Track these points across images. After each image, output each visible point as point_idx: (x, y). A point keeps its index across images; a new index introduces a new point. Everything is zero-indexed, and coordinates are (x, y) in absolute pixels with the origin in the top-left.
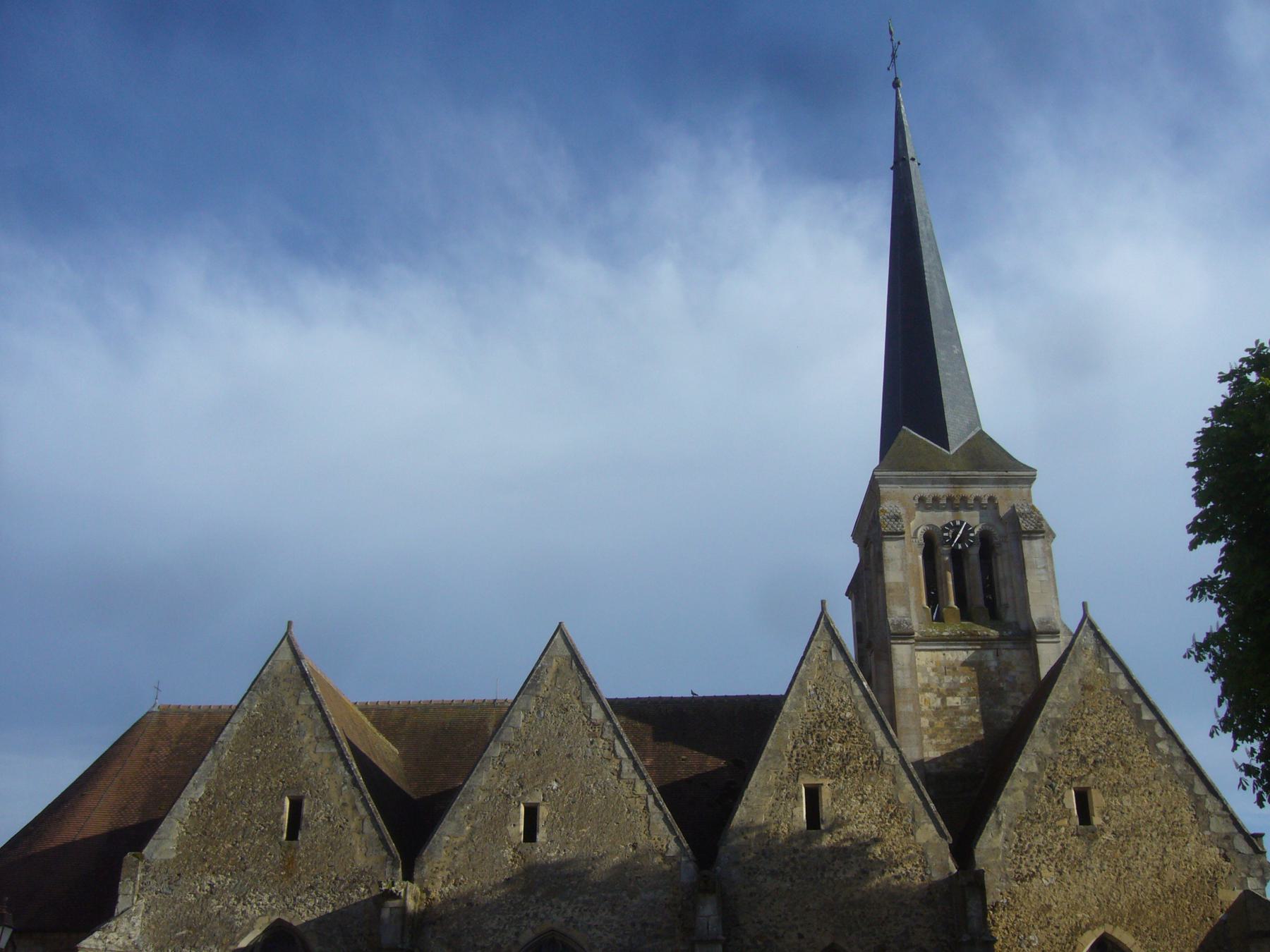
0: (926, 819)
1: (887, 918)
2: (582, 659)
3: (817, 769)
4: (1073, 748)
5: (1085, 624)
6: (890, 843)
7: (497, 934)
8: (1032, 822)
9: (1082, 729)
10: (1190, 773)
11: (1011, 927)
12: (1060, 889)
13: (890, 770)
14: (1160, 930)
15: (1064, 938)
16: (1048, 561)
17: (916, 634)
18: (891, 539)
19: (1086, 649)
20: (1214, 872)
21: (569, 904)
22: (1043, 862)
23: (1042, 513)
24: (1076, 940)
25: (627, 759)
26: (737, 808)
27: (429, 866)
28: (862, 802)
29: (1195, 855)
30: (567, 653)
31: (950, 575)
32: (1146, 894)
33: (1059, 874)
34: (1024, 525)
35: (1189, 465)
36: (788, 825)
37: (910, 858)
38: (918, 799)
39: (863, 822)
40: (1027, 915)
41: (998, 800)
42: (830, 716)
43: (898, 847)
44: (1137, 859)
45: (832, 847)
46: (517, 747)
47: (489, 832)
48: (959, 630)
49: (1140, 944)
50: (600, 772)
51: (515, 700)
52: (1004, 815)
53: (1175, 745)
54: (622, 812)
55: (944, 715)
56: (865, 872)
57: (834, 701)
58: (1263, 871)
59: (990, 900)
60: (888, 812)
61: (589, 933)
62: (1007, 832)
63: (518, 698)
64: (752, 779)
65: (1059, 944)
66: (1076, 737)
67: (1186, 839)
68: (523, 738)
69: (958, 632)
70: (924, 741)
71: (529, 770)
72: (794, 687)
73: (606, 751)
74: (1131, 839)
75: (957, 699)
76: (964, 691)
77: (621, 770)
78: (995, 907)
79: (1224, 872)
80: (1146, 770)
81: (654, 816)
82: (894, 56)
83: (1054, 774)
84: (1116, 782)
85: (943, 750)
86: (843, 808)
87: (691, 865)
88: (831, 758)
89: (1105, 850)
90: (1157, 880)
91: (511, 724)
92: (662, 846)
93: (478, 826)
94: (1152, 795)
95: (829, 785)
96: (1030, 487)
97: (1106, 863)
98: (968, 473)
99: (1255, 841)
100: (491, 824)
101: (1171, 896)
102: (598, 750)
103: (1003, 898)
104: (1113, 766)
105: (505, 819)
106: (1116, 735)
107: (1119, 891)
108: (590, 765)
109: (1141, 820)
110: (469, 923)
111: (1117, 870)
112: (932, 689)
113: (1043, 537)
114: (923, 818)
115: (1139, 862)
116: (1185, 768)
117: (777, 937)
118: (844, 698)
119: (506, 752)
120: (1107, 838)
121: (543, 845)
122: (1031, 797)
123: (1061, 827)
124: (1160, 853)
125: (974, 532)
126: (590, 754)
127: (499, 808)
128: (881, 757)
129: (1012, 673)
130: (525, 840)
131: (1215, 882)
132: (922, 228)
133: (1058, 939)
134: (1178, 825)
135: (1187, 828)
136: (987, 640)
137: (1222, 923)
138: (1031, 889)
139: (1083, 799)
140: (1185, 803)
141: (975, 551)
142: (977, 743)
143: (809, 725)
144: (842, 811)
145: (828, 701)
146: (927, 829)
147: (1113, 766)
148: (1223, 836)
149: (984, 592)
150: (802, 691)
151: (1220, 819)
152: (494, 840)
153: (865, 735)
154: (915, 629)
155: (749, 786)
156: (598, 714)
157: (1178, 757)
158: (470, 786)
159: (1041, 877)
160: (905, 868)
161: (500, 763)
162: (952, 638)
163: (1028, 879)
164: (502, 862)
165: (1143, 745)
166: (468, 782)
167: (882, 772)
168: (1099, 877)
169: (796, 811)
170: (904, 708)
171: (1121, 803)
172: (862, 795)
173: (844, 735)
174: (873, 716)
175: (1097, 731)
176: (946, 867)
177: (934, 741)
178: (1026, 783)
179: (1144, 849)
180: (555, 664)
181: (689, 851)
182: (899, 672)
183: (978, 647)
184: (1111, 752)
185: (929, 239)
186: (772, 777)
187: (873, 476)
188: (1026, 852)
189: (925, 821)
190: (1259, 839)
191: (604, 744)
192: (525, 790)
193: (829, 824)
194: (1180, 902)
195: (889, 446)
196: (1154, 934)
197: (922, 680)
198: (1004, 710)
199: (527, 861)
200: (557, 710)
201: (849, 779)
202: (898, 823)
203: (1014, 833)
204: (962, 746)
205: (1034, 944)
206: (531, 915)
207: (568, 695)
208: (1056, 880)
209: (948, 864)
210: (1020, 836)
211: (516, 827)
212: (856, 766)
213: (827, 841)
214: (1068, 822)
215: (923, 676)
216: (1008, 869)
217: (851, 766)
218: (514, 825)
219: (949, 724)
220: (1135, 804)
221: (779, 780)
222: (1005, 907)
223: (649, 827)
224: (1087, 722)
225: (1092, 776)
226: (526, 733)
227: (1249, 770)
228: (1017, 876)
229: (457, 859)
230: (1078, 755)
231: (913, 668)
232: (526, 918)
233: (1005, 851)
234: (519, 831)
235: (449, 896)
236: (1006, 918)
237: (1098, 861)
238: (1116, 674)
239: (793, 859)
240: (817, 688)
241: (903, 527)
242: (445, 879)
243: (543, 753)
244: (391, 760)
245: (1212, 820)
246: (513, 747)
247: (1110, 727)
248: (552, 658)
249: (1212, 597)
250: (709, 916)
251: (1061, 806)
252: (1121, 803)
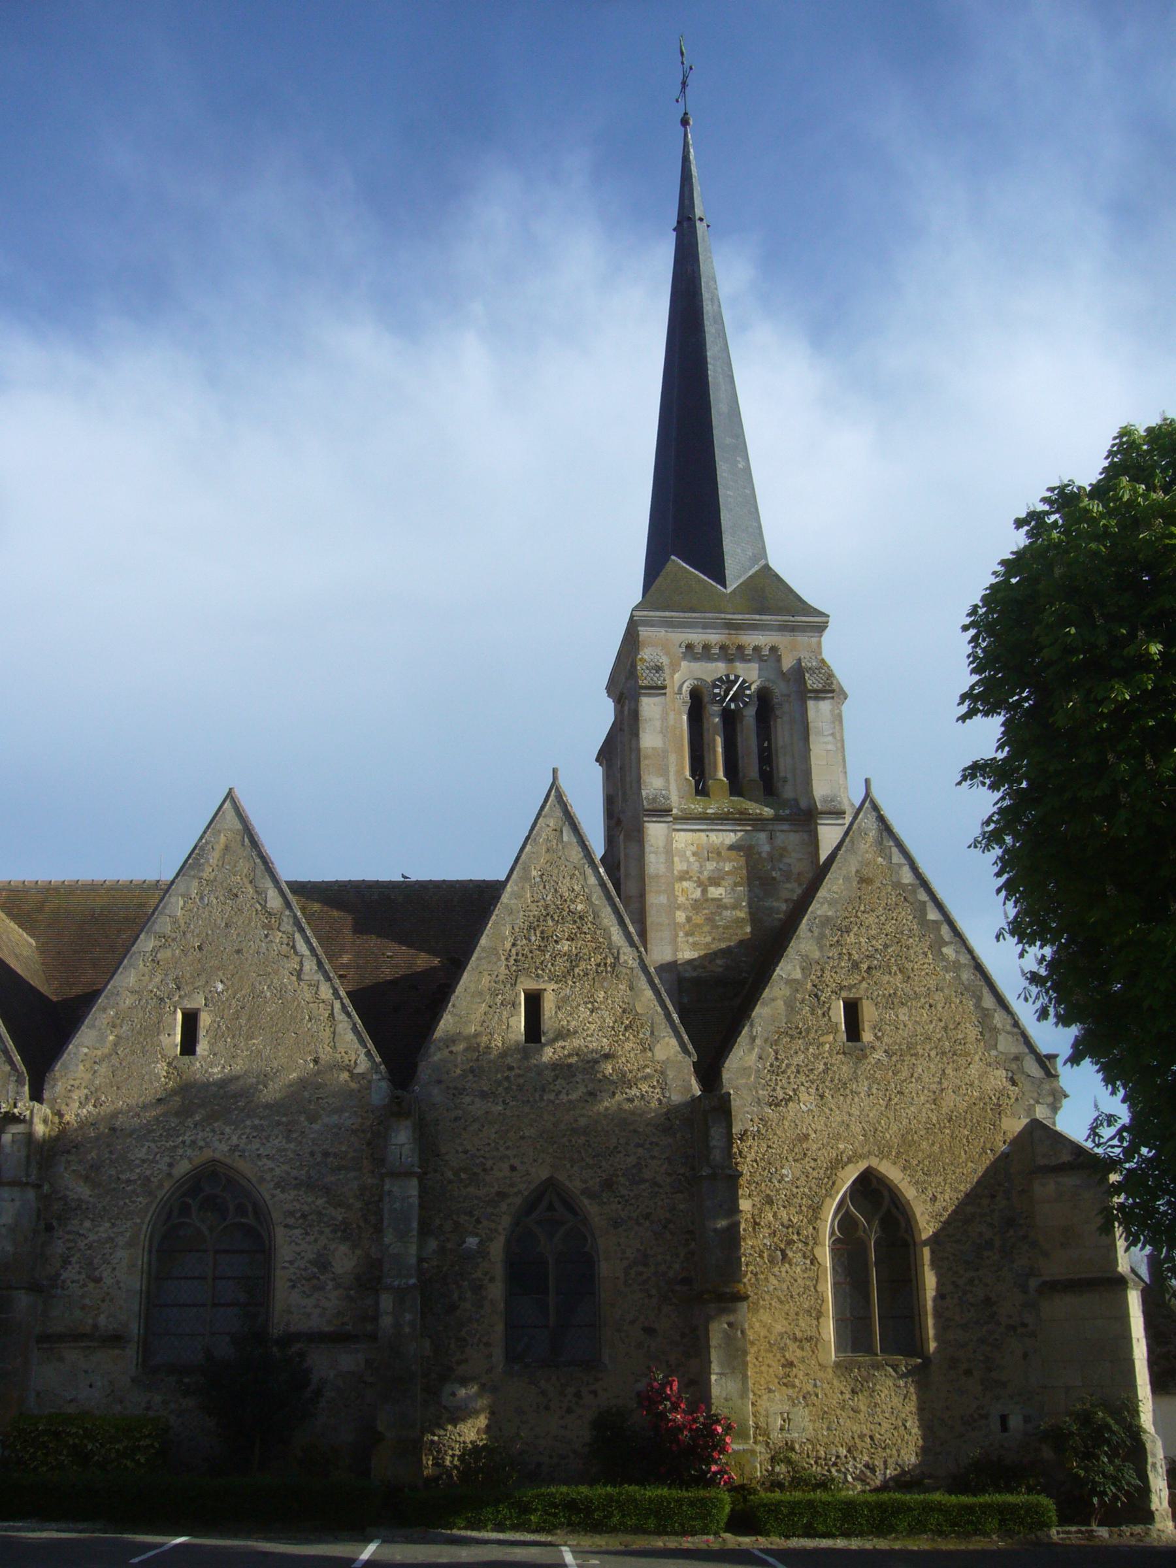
0: (668, 1032)
1: (616, 1147)
2: (256, 834)
3: (540, 972)
4: (844, 951)
5: (867, 804)
6: (624, 1060)
7: (145, 1166)
8: (792, 1037)
9: (856, 929)
10: (978, 983)
11: (761, 1159)
12: (820, 1116)
13: (627, 974)
14: (933, 1164)
15: (822, 1172)
16: (837, 728)
17: (675, 811)
18: (650, 695)
19: (866, 834)
20: (999, 1098)
21: (235, 1129)
22: (802, 1084)
23: (832, 668)
24: (836, 1175)
25: (310, 957)
26: (442, 1017)
27: (63, 1083)
28: (592, 1012)
29: (979, 1078)
30: (239, 826)
31: (719, 741)
32: (919, 1122)
33: (819, 1098)
34: (811, 682)
35: (965, 628)
36: (503, 1037)
37: (646, 1078)
38: (659, 1009)
39: (592, 1035)
40: (780, 1146)
41: (752, 1011)
42: (558, 908)
43: (633, 1065)
44: (912, 1082)
45: (554, 1064)
46: (174, 939)
47: (138, 1043)
48: (726, 807)
49: (909, 1180)
50: (276, 972)
51: (173, 882)
52: (760, 1028)
53: (963, 950)
54: (302, 1020)
55: (705, 909)
56: (592, 1094)
57: (564, 890)
58: (1054, 1098)
59: (736, 1129)
60: (622, 1023)
61: (260, 1163)
62: (762, 1048)
63: (176, 881)
64: (462, 982)
65: (816, 1179)
66: (848, 938)
67: (969, 1060)
68: (181, 929)
69: (726, 810)
70: (679, 939)
71: (188, 968)
72: (515, 873)
73: (284, 946)
74: (905, 1058)
75: (721, 890)
76: (727, 883)
77: (301, 970)
78: (743, 1136)
79: (1010, 1098)
80: (928, 979)
81: (341, 1025)
82: (684, 84)
83: (820, 981)
84: (892, 992)
85: (702, 950)
86: (568, 1019)
87: (384, 1084)
88: (557, 958)
89: (875, 1071)
90: (933, 1106)
91: (167, 912)
92: (350, 1061)
93: (124, 1036)
94: (933, 1008)
95: (553, 990)
96: (821, 636)
97: (875, 1086)
98: (747, 616)
99: (1048, 1063)
100: (139, 1033)
101: (948, 1125)
102: (274, 944)
103: (753, 1126)
104: (890, 974)
105: (159, 1027)
106: (895, 936)
107: (888, 1119)
108: (264, 963)
109: (919, 1037)
110: (111, 1152)
111: (888, 1095)
112: (691, 877)
113: (833, 698)
114: (665, 1031)
115: (913, 1085)
116: (972, 977)
117: (485, 1170)
118: (575, 887)
119: (160, 947)
120: (877, 1057)
121: (204, 1058)
122: (792, 1008)
123: (826, 1043)
124: (937, 1075)
125: (750, 690)
126: (263, 950)
127: (150, 1014)
128: (617, 958)
129: (787, 860)
130: (182, 1053)
131: (998, 1109)
132: (708, 308)
133: (815, 1174)
134: (960, 1043)
135: (971, 1048)
136: (760, 820)
137: (1005, 1156)
138: (786, 1115)
139: (852, 1010)
140: (971, 1019)
141: (750, 712)
142: (741, 942)
143: (532, 918)
144: (568, 1021)
145: (556, 890)
146: (668, 1044)
147: (890, 974)
148: (1012, 1057)
149: (759, 763)
150: (526, 877)
151: (1010, 1038)
152: (144, 1053)
153: (598, 932)
154: (673, 805)
155: (457, 990)
156: (274, 901)
157: (965, 965)
158: (115, 987)
159: (800, 1101)
160: (640, 1089)
161: (153, 960)
162: (717, 816)
163: (783, 1103)
164: (153, 1078)
165: (926, 950)
166: (112, 982)
167: (617, 976)
168: (866, 1103)
169: (512, 1021)
170: (656, 900)
171: (897, 1016)
172: (592, 1003)
173: (574, 931)
174: (609, 909)
175: (873, 932)
176: (688, 1088)
177: (691, 940)
178: (787, 992)
179: (920, 1070)
180: (222, 839)
181: (383, 1067)
182: (652, 856)
184: (888, 957)
185: (715, 322)
186: (485, 980)
187: (632, 616)
188: (783, 1073)
189: (665, 1034)
190: (1051, 1060)
191: (281, 937)
192: (182, 993)
193: (551, 1035)
194: (957, 1133)
195: (657, 575)
196: (926, 1169)
197: (679, 866)
198: (775, 904)
199: (184, 1077)
200: (224, 895)
201: (578, 984)
202: (634, 1036)
203: (770, 1050)
204: (723, 945)
205: (787, 1179)
206: (188, 1142)
207: (239, 877)
208: (816, 1106)
209: (691, 1085)
210: (777, 1054)
211: (171, 1037)
212: (587, 969)
213: (548, 1054)
214: (834, 1038)
215: (681, 862)
216: (761, 1092)
217: (581, 968)
218: (169, 1035)
219: (709, 919)
220: (913, 1018)
221: (494, 984)
222: (754, 1136)
223: (334, 1038)
224: (862, 921)
225: (864, 985)
226: (185, 923)
227: (1034, 978)
228: (771, 1099)
229: (97, 1074)
230: (849, 960)
231: (669, 852)
232: (181, 1145)
233: (758, 1071)
234: (174, 1042)
235: (87, 1119)
236: (756, 1148)
237: (866, 1084)
238: (900, 866)
239: (507, 1078)
240: (543, 874)
241: (664, 680)
242: (83, 1099)
243: (206, 947)
244: (25, 953)
245: (1001, 1038)
246: (169, 940)
247: (888, 928)
248: (219, 832)
249: (985, 783)
250: (403, 1145)
251: (826, 1019)
252: (897, 1016)
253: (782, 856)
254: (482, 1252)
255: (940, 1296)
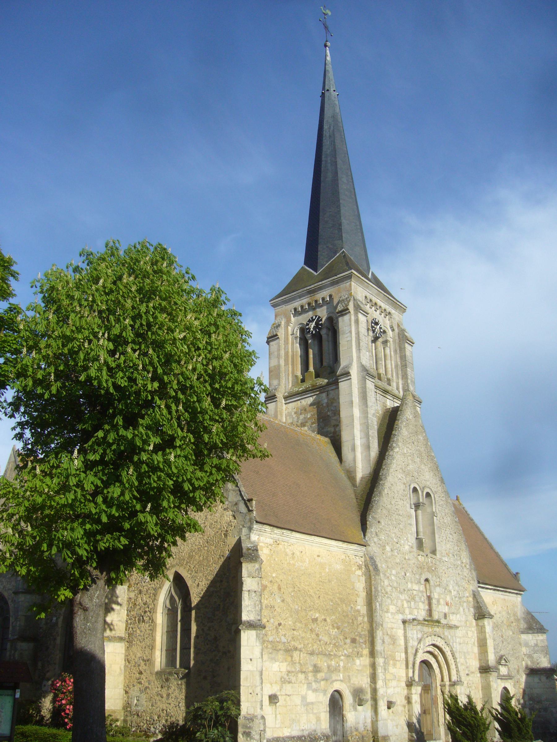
76: (309, 424)
136: (321, 387)
183: (318, 393)
198: (329, 429)
253: (332, 403)
254: (56, 623)
255: (197, 637)
